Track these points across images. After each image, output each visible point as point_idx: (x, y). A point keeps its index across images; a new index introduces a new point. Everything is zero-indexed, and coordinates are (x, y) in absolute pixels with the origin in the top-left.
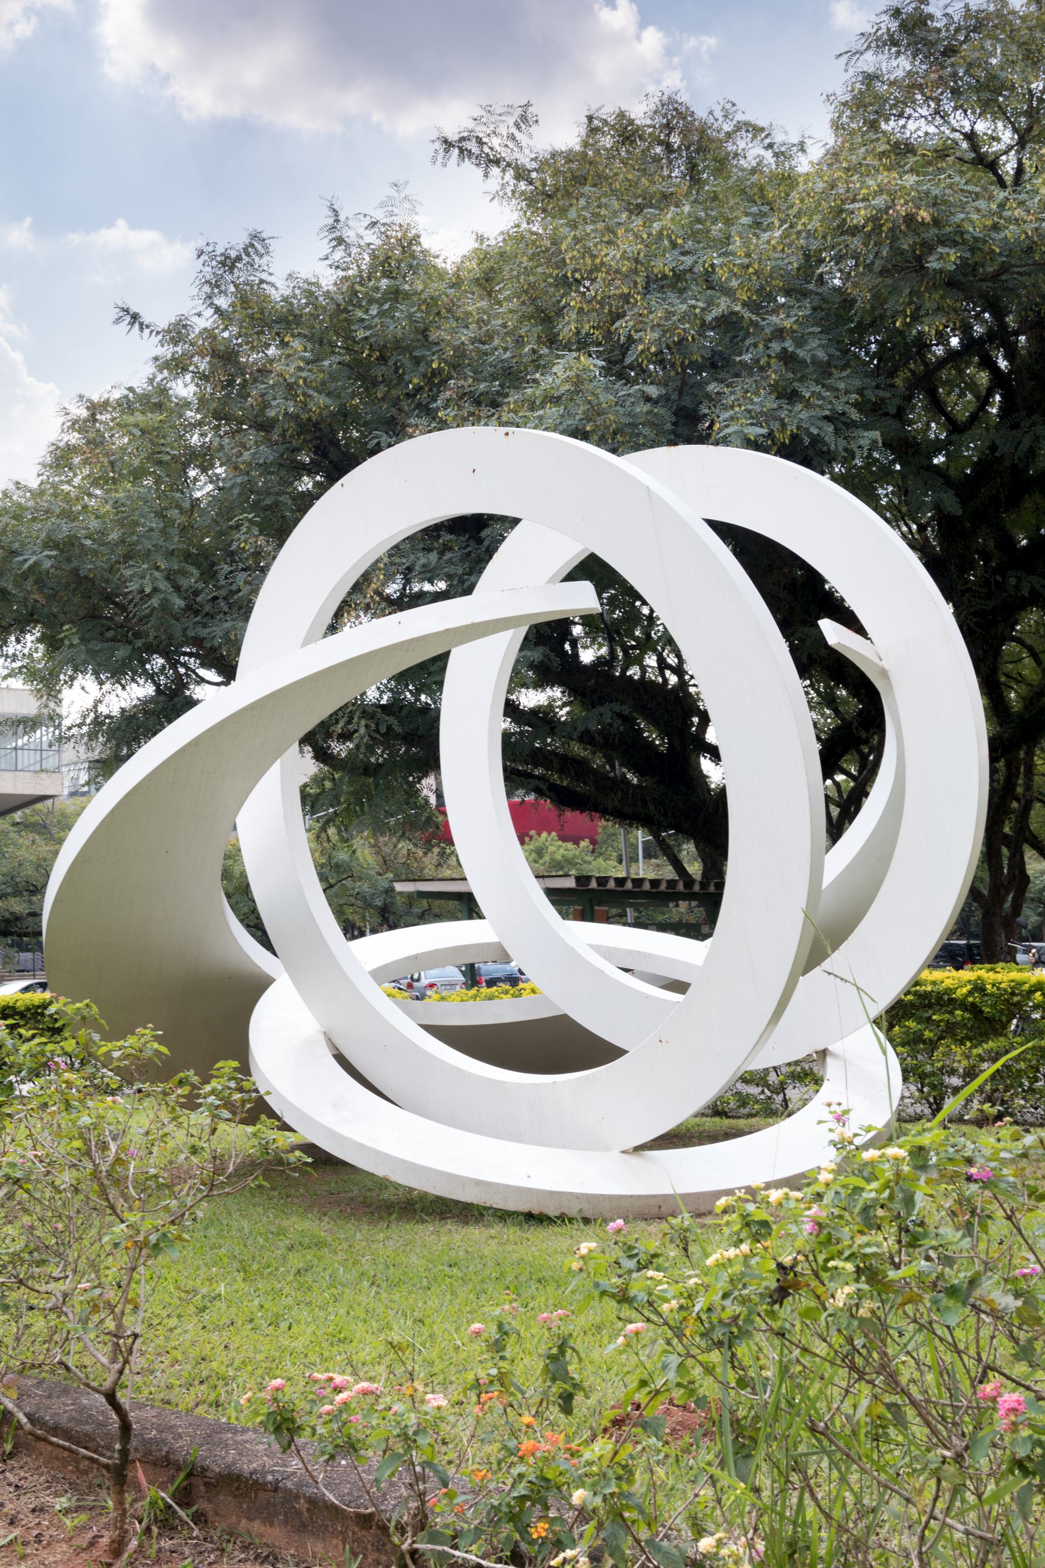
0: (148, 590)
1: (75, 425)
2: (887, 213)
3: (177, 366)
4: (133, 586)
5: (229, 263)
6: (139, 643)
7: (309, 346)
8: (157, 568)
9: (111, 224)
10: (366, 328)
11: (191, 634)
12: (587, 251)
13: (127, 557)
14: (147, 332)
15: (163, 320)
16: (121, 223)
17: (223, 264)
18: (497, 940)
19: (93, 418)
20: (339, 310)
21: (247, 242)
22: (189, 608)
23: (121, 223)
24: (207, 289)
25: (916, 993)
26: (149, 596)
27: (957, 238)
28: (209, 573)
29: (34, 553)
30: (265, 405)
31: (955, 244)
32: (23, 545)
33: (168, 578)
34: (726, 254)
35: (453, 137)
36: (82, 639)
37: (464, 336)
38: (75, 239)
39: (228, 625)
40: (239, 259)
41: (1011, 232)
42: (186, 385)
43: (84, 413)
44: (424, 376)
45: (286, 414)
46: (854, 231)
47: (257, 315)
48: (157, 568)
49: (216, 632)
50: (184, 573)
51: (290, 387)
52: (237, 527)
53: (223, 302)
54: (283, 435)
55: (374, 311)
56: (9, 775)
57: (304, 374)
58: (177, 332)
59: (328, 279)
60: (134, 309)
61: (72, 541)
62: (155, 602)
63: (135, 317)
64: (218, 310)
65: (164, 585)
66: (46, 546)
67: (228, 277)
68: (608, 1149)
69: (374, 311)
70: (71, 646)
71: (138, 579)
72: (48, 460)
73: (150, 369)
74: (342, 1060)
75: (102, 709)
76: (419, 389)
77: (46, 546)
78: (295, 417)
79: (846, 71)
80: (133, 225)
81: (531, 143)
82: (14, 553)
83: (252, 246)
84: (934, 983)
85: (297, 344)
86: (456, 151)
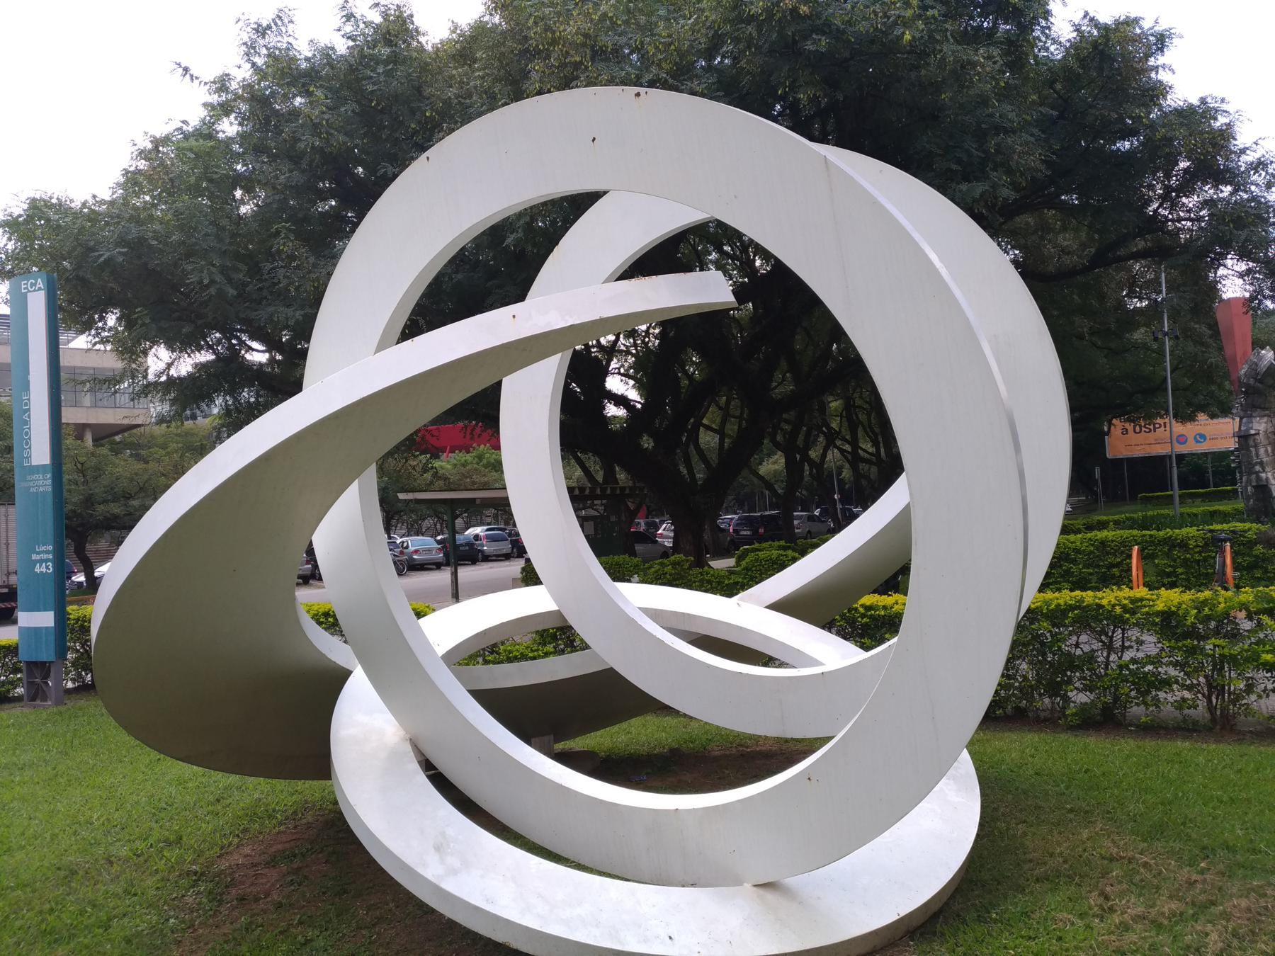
0: (206, 281)
1: (142, 154)
2: (778, 6)
3: (224, 109)
4: (193, 278)
5: (262, 31)
6: (200, 322)
7: (329, 95)
8: (213, 265)
10: (374, 84)
11: (242, 315)
12: (547, 29)
13: (189, 255)
14: (196, 82)
15: (211, 74)
17: (257, 30)
18: (556, 608)
19: (156, 148)
20: (352, 69)
22: (239, 295)
24: (244, 48)
26: (208, 286)
27: (825, 28)
28: (255, 270)
29: (108, 250)
30: (297, 140)
31: (824, 33)
32: (98, 243)
33: (222, 273)
34: (652, 35)
36: (153, 320)
37: (451, 93)
39: (271, 309)
40: (269, 27)
41: (863, 27)
42: (231, 124)
43: (149, 146)
44: (419, 122)
45: (313, 147)
46: (751, 19)
47: (284, 71)
48: (213, 265)
49: (599, 507)
50: (237, 270)
51: (315, 126)
52: (278, 233)
53: (260, 61)
54: (310, 165)
55: (380, 70)
56: (110, 411)
57: (326, 116)
58: (221, 84)
59: (342, 47)
61: (141, 241)
62: (213, 291)
63: (186, 70)
64: (254, 64)
65: (218, 278)
66: (117, 245)
67: (261, 42)
68: (737, 881)
69: (380, 70)
70: (143, 324)
71: (197, 274)
72: (122, 180)
73: (203, 113)
74: (428, 766)
75: (173, 372)
76: (415, 133)
77: (117, 245)
78: (321, 150)
82: (92, 249)
83: (280, 18)
84: (885, 607)
85: (319, 93)
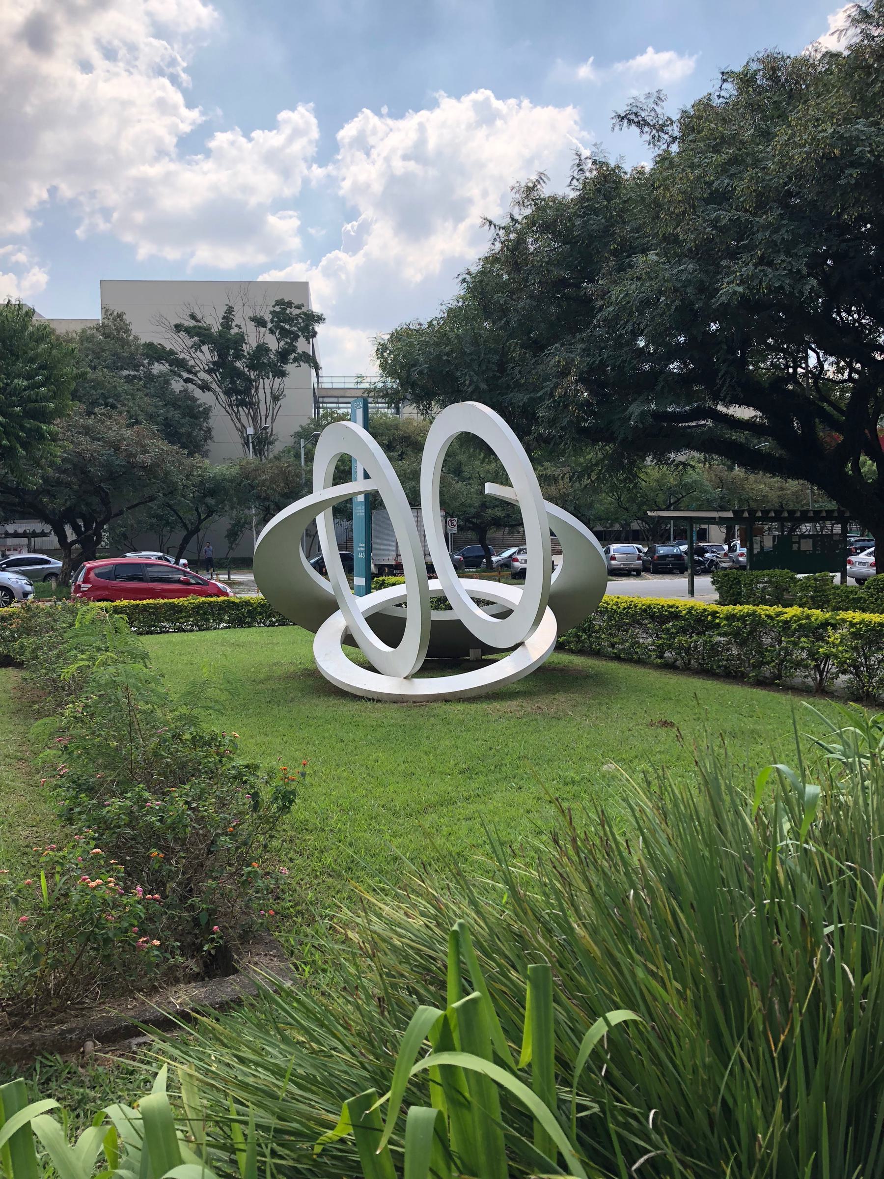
9: (643, 52)
16: (650, 50)
21: (537, 178)
23: (650, 50)
25: (669, 612)
35: (623, 115)
38: (619, 67)
60: (489, 218)
63: (491, 222)
79: (839, 41)
80: (657, 51)
81: (663, 111)
86: (626, 121)
